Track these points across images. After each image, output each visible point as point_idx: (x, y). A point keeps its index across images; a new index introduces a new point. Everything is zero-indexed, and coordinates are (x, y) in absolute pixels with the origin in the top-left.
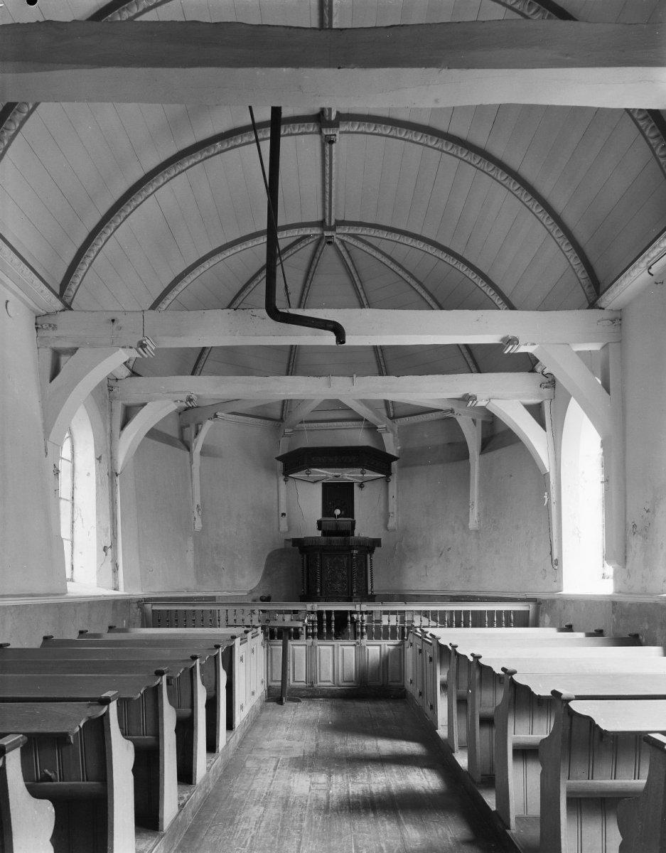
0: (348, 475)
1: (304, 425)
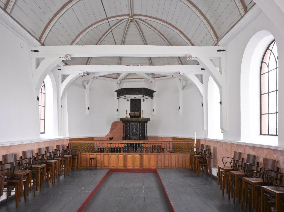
0: (139, 97)
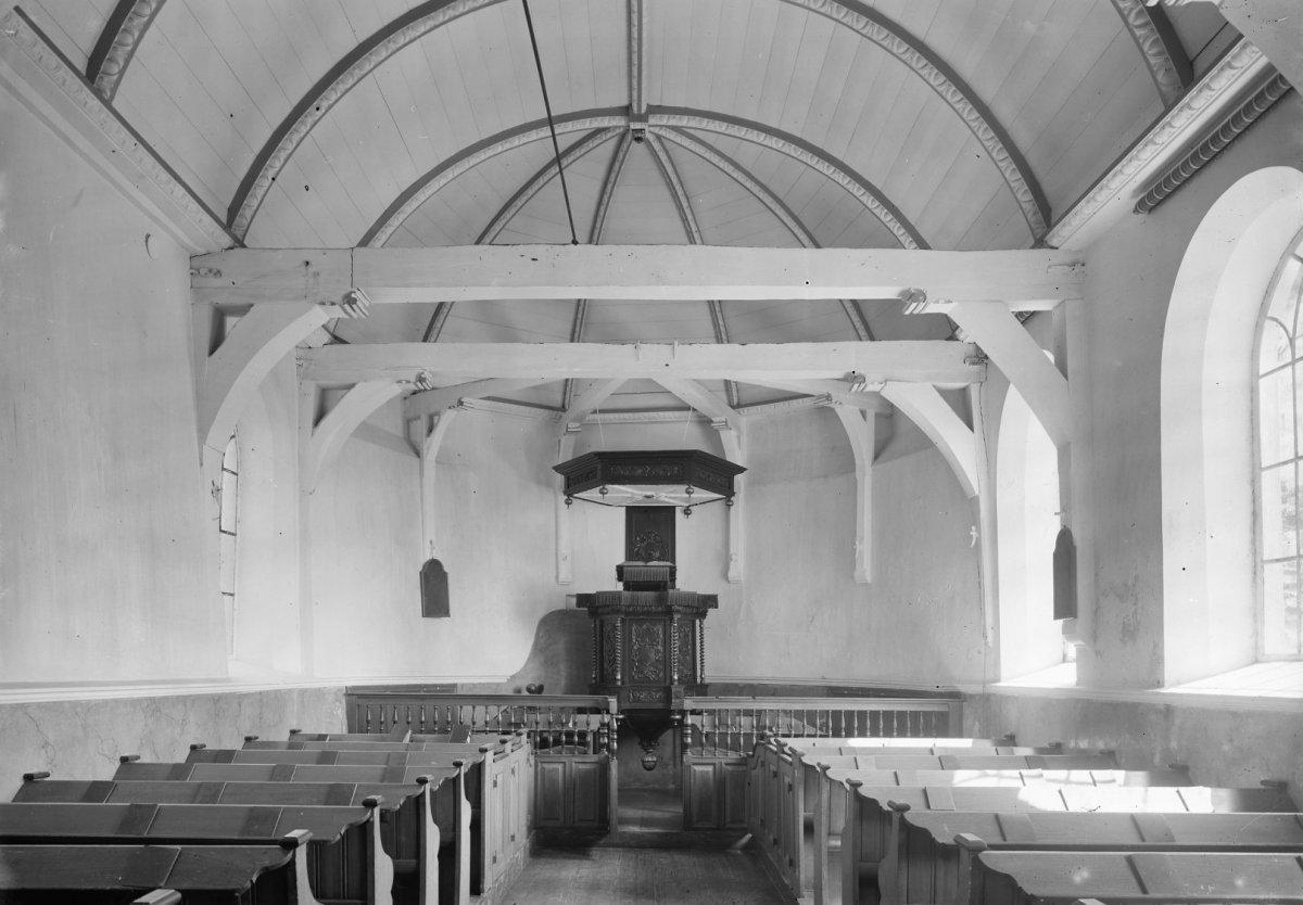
0: (666, 495)
1: (598, 417)
